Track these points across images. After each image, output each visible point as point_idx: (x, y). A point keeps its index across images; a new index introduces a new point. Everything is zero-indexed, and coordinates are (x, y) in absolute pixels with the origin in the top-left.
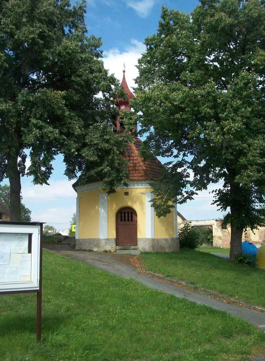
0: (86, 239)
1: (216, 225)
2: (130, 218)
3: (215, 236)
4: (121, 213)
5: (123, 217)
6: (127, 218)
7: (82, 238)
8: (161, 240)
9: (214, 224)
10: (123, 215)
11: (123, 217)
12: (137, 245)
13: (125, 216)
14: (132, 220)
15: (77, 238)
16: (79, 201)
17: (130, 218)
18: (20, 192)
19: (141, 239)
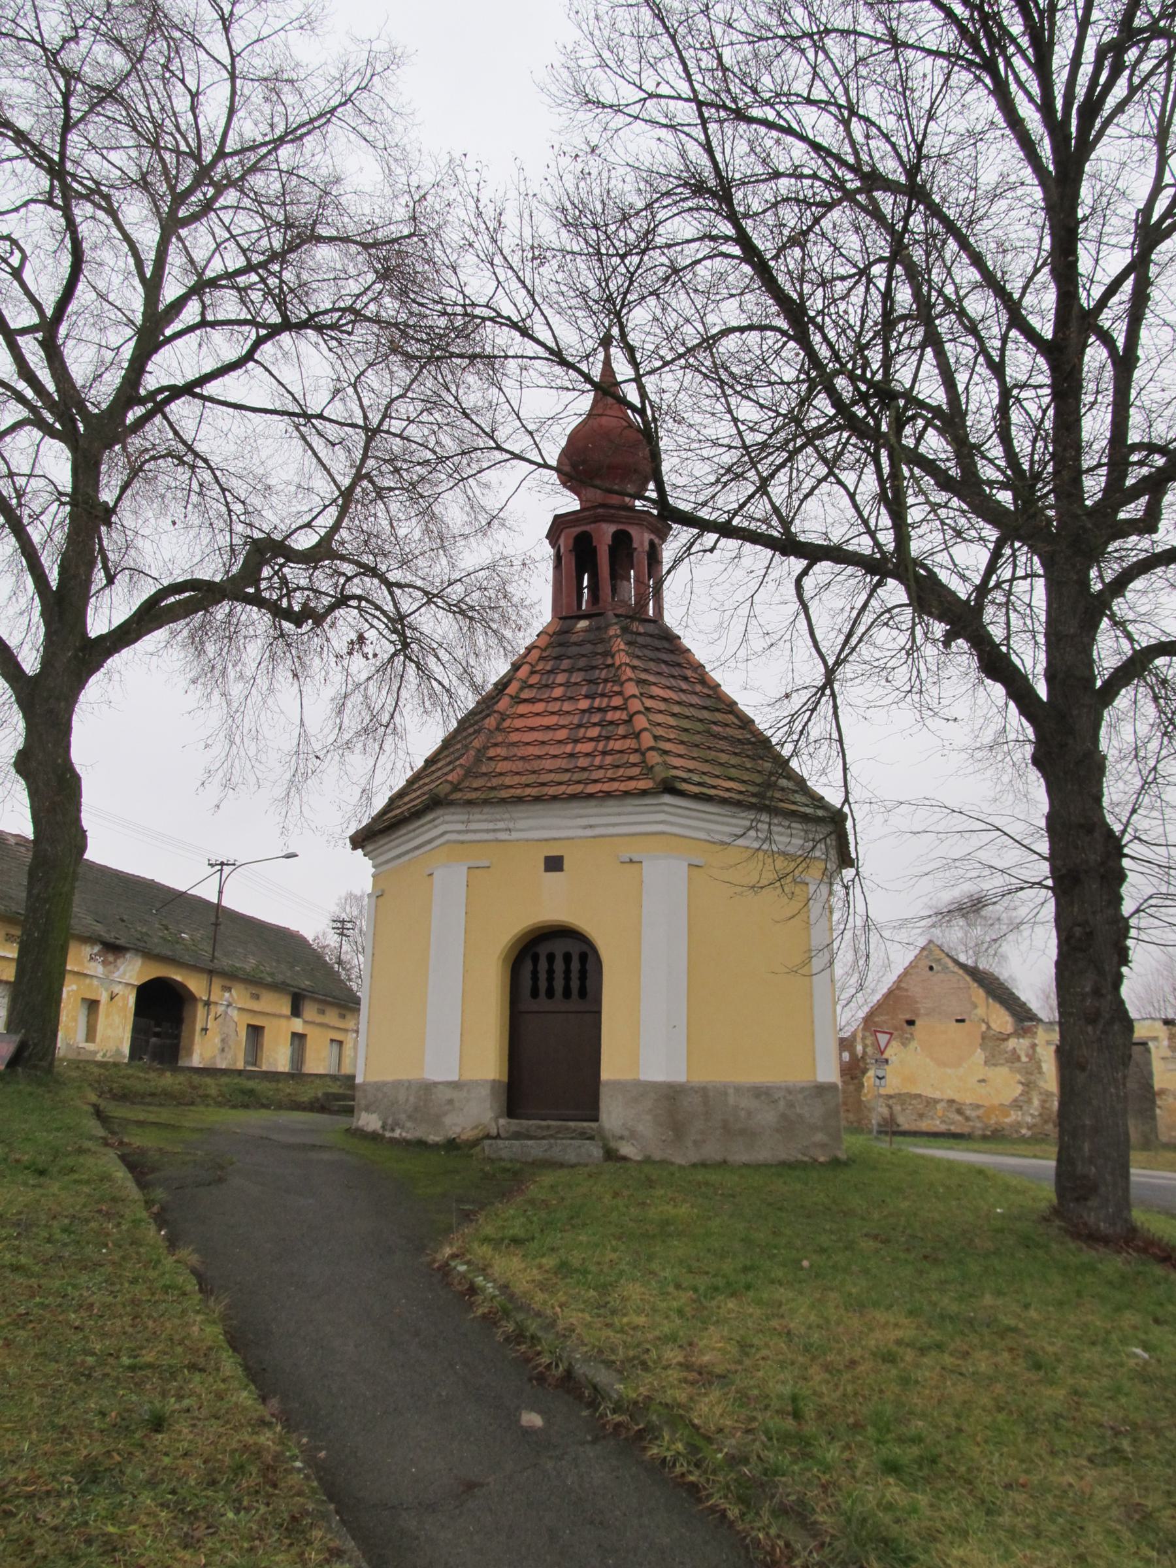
0: (385, 1084)
1: (1166, 1043)
2: (575, 984)
3: (1163, 1092)
4: (535, 959)
5: (543, 976)
6: (559, 984)
7: (374, 1078)
8: (726, 1094)
9: (1155, 1039)
10: (543, 965)
11: (543, 976)
12: (596, 1119)
13: (551, 972)
14: (583, 993)
15: (359, 1080)
16: (629, 1433)
17: (575, 984)
18: (74, 504)
19: (619, 1086)
